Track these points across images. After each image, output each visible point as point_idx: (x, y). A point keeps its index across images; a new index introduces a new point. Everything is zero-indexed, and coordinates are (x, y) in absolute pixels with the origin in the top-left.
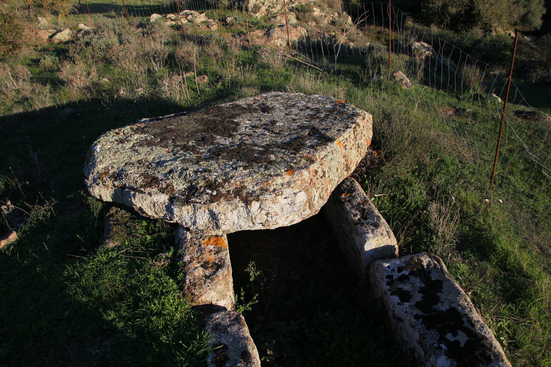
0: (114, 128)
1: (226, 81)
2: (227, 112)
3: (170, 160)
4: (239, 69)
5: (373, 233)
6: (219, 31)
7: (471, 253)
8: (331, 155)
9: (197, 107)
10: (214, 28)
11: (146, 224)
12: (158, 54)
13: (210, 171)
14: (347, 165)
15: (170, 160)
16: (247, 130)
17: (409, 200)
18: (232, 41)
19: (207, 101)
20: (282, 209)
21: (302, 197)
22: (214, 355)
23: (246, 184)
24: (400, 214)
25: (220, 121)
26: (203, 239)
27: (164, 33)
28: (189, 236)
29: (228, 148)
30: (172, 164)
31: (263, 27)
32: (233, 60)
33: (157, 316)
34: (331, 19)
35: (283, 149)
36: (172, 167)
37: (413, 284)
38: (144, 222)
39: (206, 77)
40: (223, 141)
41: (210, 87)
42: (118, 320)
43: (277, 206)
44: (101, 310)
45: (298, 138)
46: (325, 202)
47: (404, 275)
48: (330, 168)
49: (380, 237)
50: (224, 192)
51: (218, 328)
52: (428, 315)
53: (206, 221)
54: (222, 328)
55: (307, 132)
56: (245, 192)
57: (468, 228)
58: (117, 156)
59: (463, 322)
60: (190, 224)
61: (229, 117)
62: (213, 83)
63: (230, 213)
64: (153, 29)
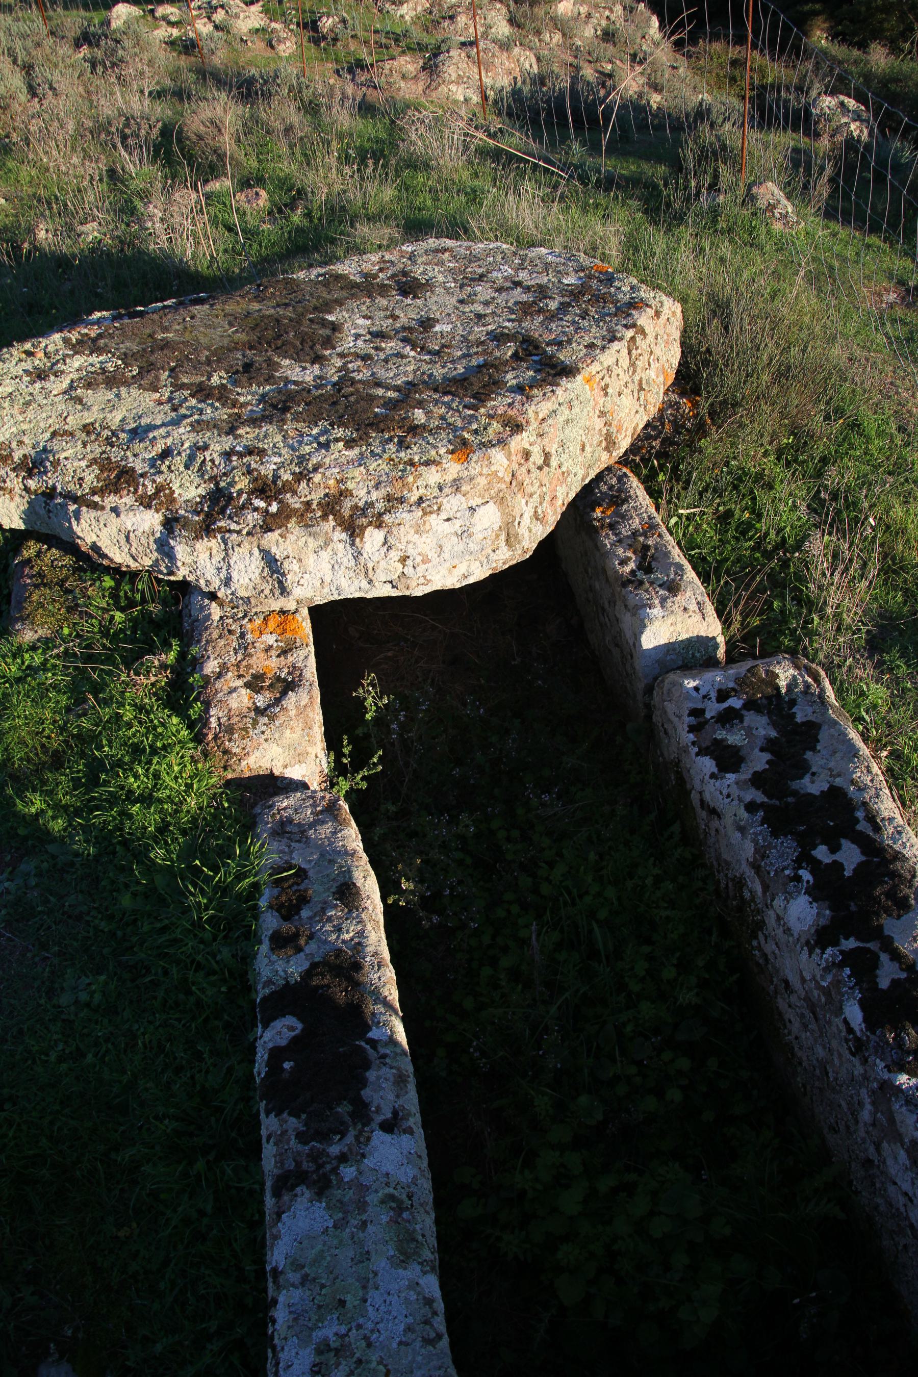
0: (22, 339)
1: (315, 206)
2: (311, 295)
3: (164, 425)
4: (347, 170)
5: (662, 607)
6: (300, 56)
7: (900, 657)
8: (567, 412)
9: (239, 276)
10: (287, 48)
11: (112, 583)
12: (134, 127)
13: (262, 452)
15: (164, 425)
16: (360, 343)
17: (762, 526)
18: (332, 88)
19: (265, 259)
20: (440, 547)
21: (489, 517)
22: (276, 891)
23: (350, 485)
24: (738, 560)
25: (291, 320)
26: (250, 620)
27: (151, 63)
28: (216, 612)
29: (309, 391)
30: (168, 434)
31: (421, 47)
32: (334, 143)
33: (142, 802)
34: (604, 23)
35: (446, 393)
36: (169, 441)
37: (749, 732)
38: (107, 578)
39: (263, 193)
40: (296, 372)
41: (274, 221)
42: (50, 813)
43: (428, 541)
44: (10, 791)
45: (486, 365)
46: (550, 529)
47: (730, 708)
48: (562, 445)
49: (679, 616)
50: (297, 506)
51: (285, 830)
52: (777, 803)
54: (296, 830)
55: (510, 349)
56: (347, 504)
57: (900, 597)
58: (30, 414)
59: (857, 821)
60: (216, 583)
61: (316, 308)
62: (280, 211)
63: (312, 557)
64: (120, 52)
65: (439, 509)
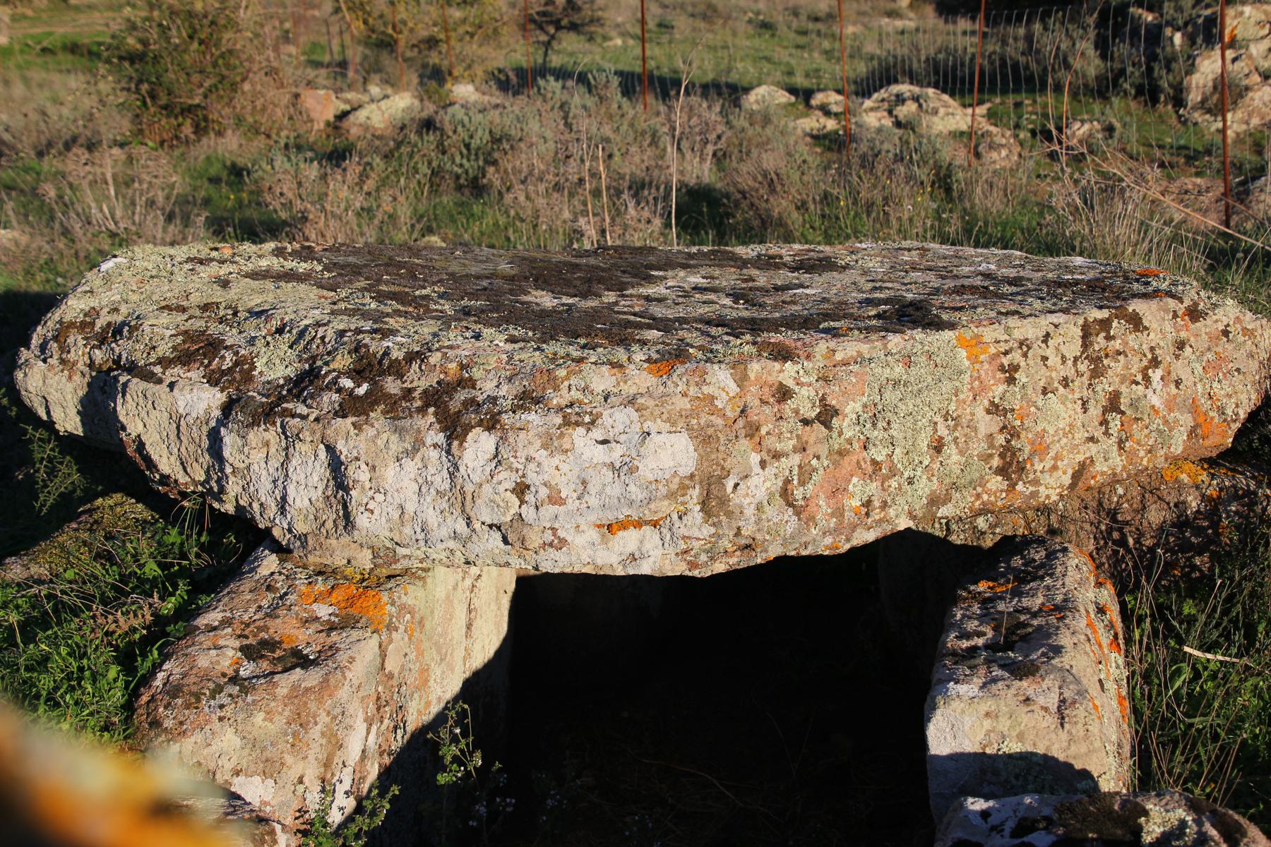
14: (1008, 452)
20: (584, 483)
23: (477, 373)
50: (393, 391)
53: (317, 495)
65: (593, 422)
